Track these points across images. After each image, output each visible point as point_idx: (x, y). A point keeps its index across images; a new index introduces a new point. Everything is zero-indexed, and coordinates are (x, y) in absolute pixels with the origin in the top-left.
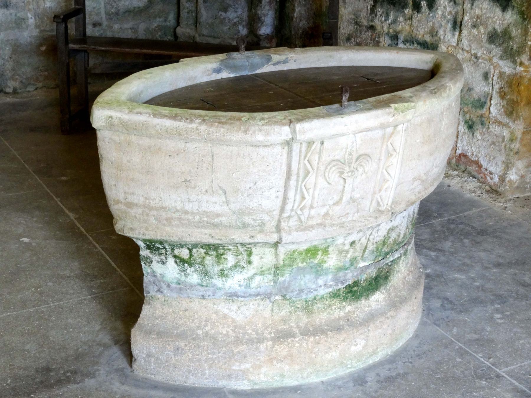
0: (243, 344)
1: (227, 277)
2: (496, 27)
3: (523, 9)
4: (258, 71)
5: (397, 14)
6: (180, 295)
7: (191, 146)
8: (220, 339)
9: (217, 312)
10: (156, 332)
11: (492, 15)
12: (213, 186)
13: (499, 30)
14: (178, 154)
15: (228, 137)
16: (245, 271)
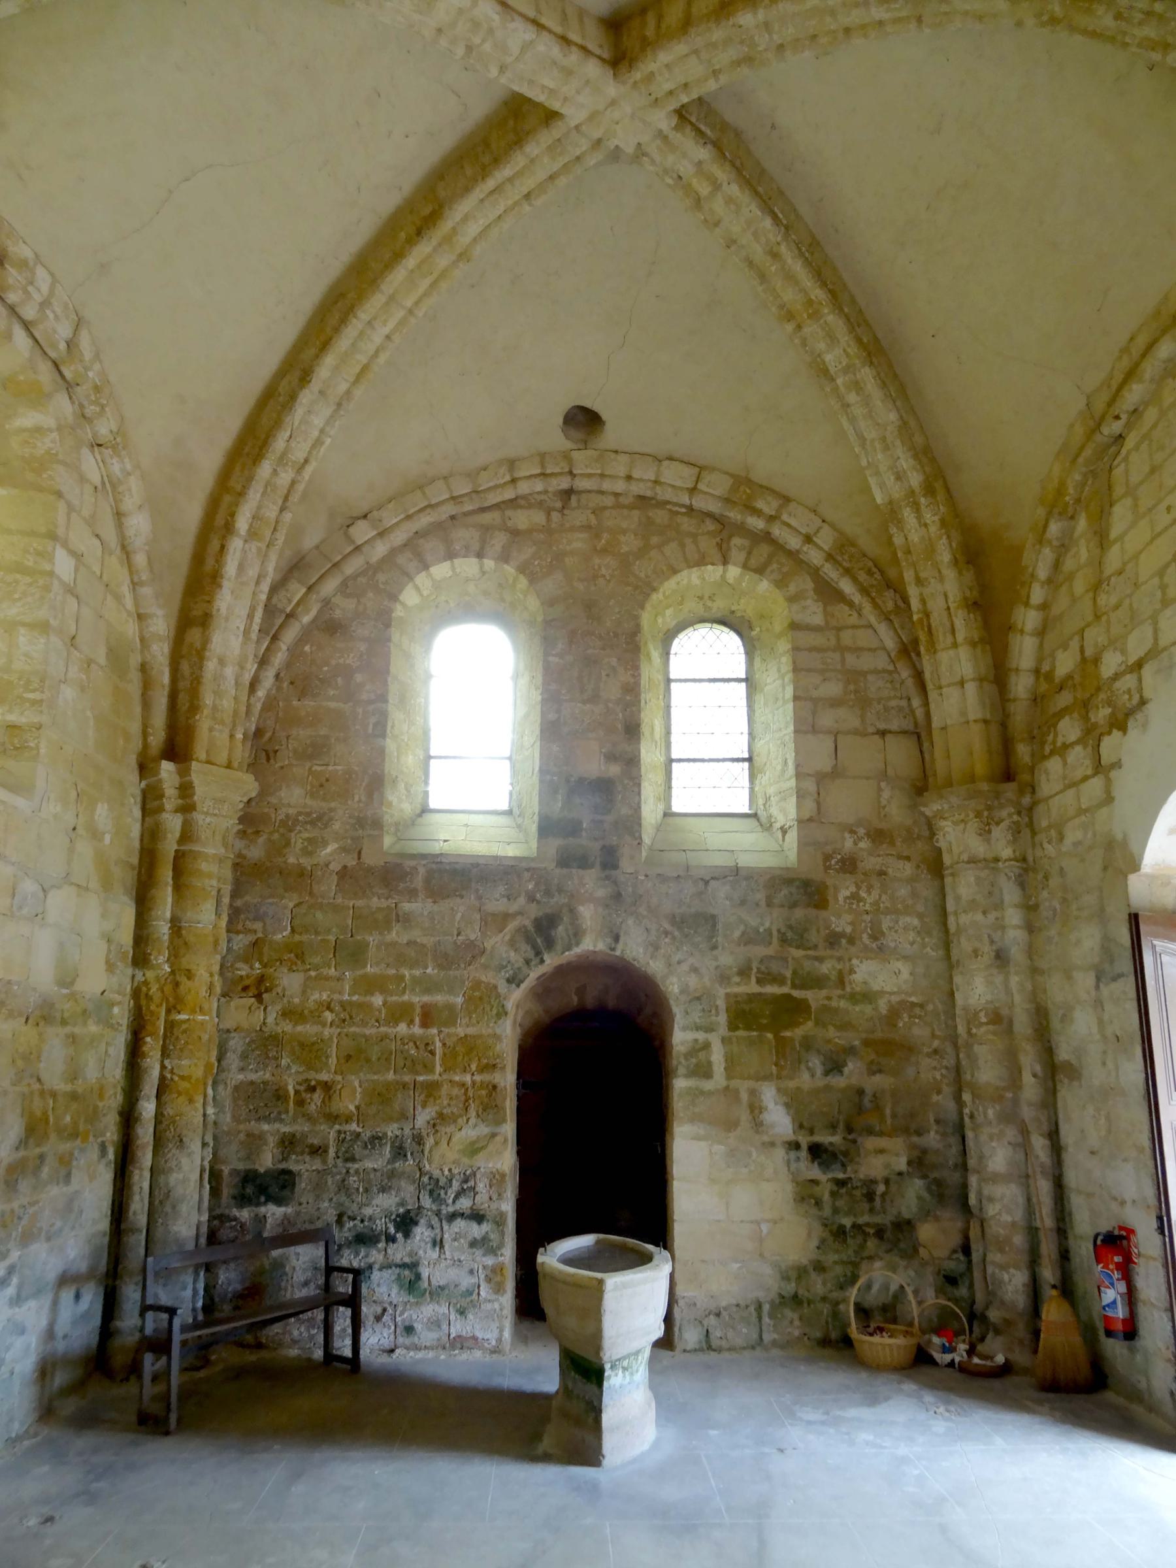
12: (24, 1020)
13: (478, 1238)
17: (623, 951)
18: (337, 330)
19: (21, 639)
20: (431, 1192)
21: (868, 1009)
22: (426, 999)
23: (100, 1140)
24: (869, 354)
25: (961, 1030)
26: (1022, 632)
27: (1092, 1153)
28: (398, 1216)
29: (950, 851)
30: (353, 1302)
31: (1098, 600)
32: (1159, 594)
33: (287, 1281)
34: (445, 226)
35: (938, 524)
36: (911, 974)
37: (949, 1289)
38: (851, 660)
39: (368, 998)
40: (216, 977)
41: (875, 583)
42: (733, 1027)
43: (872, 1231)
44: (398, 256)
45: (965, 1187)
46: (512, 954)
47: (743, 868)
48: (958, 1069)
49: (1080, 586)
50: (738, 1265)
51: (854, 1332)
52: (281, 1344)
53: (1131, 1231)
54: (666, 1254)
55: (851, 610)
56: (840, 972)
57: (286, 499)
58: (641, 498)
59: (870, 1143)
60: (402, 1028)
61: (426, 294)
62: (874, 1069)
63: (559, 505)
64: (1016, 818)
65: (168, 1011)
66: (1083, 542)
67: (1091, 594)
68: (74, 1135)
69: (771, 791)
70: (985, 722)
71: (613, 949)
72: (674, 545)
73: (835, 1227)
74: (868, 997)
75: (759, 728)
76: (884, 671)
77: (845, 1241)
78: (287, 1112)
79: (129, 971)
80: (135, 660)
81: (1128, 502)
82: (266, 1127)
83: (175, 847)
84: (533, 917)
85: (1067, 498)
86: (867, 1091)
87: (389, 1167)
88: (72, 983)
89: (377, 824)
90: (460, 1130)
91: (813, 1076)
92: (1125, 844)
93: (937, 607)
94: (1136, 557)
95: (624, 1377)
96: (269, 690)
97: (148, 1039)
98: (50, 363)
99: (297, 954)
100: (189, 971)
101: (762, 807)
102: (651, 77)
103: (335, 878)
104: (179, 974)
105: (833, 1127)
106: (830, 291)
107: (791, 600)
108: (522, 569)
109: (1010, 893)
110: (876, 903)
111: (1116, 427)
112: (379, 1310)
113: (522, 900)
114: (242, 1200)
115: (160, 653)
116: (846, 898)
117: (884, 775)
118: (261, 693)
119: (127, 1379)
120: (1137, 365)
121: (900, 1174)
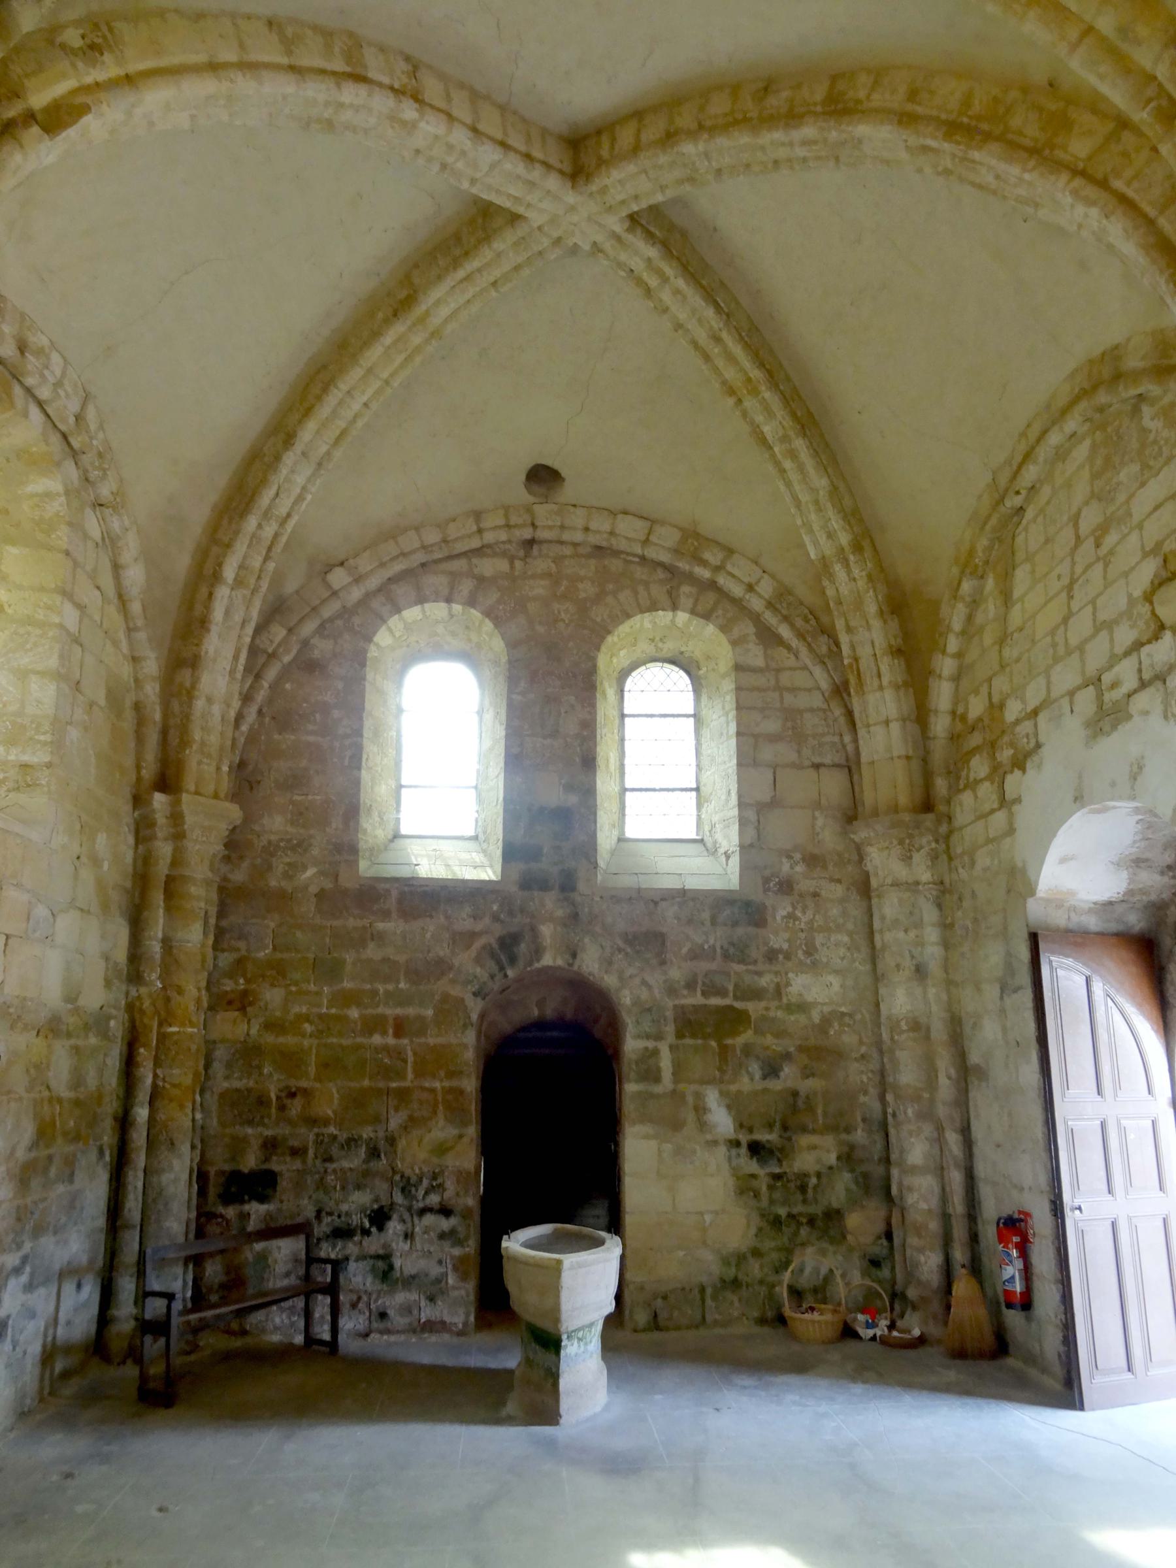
17: (579, 967)
18: (319, 398)
19: (33, 685)
20: (403, 1190)
21: (802, 1019)
22: (399, 1011)
23: (98, 1143)
24: (803, 427)
25: (885, 1036)
26: (940, 676)
27: (998, 1146)
28: (372, 1211)
29: (876, 875)
30: (332, 1290)
31: (1004, 651)
32: (1051, 651)
33: (270, 1272)
34: (419, 310)
35: (865, 579)
36: (841, 986)
37: (874, 1270)
38: (789, 699)
39: (345, 1010)
40: (204, 992)
41: (810, 629)
42: (680, 1035)
43: (804, 1221)
44: (376, 335)
45: (888, 1178)
46: (478, 970)
47: (690, 890)
48: (882, 1073)
49: (988, 639)
50: (683, 1253)
51: (787, 1312)
52: (264, 1331)
53: (1028, 1215)
54: (617, 1239)
55: (789, 653)
56: (778, 985)
57: (270, 549)
58: (599, 548)
59: (805, 1140)
60: (377, 1039)
61: (402, 366)
62: (807, 1073)
63: (522, 553)
64: (934, 845)
65: (160, 1025)
66: (991, 600)
67: (997, 647)
68: (77, 1138)
69: (716, 818)
70: (908, 758)
71: (571, 965)
72: (627, 592)
73: (771, 1218)
74: (802, 1007)
75: (705, 761)
76: (819, 709)
77: (780, 1230)
78: (269, 1117)
79: (124, 987)
80: (128, 703)
81: (1027, 567)
82: (250, 1131)
83: (166, 872)
84: (497, 935)
85: (977, 560)
86: (801, 1093)
87: (364, 1166)
88: (76, 999)
89: (353, 850)
90: (430, 1132)
91: (752, 1079)
92: (1024, 871)
93: (865, 652)
94: (1033, 616)
95: (579, 1346)
96: (251, 726)
97: (142, 1050)
98: (59, 435)
99: (278, 970)
100: (179, 986)
101: (708, 834)
102: (604, 190)
103: (314, 900)
104: (170, 988)
105: (770, 1126)
106: (768, 371)
107: (734, 643)
108: (488, 614)
109: (930, 914)
110: (811, 922)
111: (1018, 501)
112: (355, 1298)
113: (487, 920)
114: (228, 1198)
115: (152, 691)
116: (785, 917)
117: (817, 805)
118: (244, 728)
119: (124, 1362)
120: (1033, 448)
121: (831, 1168)
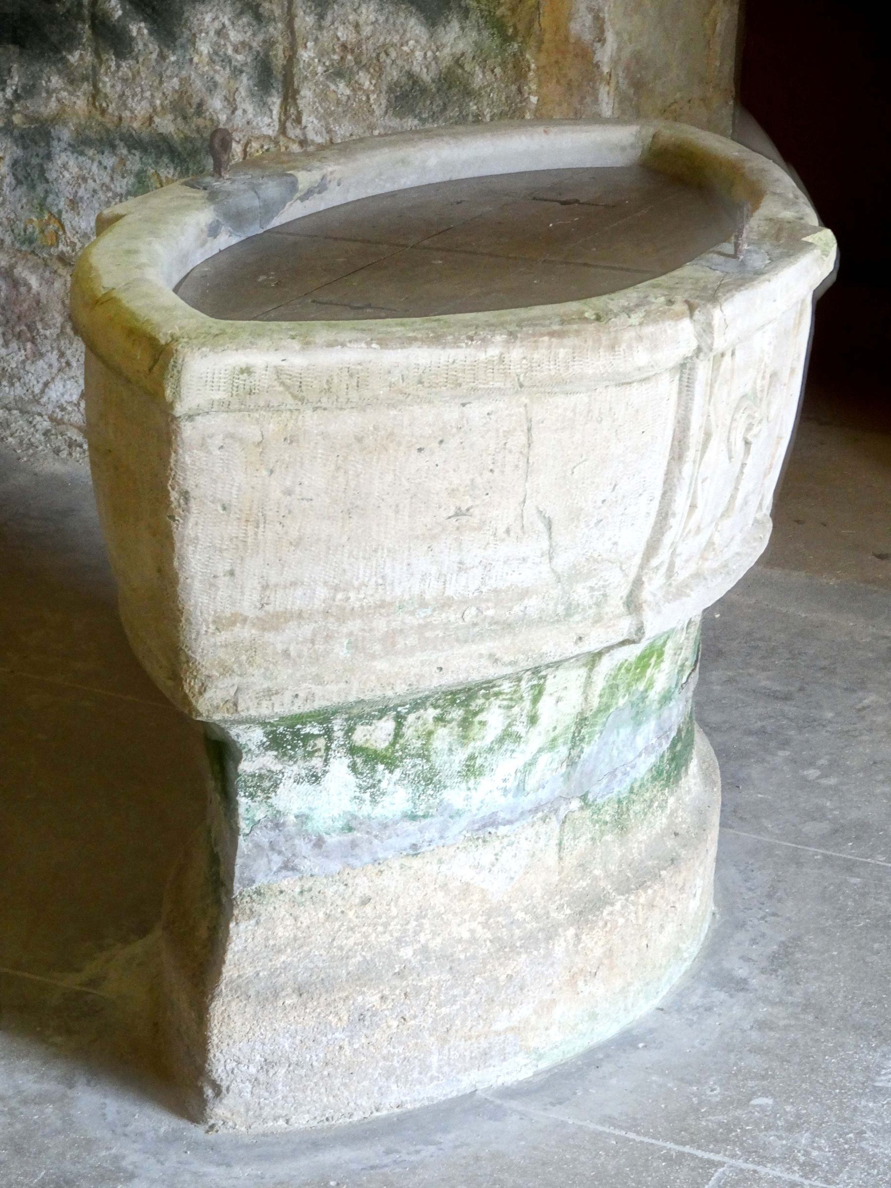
0: (519, 953)
1: (480, 774)
2: (416, 69)
3: (498, 13)
4: (276, 222)
5: (36, 68)
6: (351, 861)
7: (476, 411)
8: (462, 956)
9: (446, 884)
10: (289, 990)
11: (396, 39)
14: (441, 442)
15: (576, 368)
16: (522, 746)
